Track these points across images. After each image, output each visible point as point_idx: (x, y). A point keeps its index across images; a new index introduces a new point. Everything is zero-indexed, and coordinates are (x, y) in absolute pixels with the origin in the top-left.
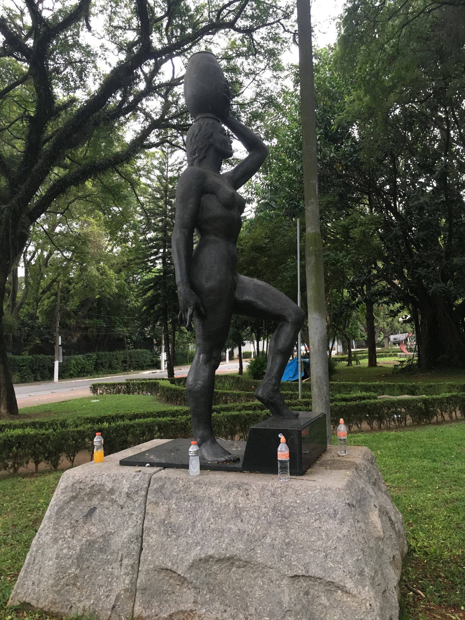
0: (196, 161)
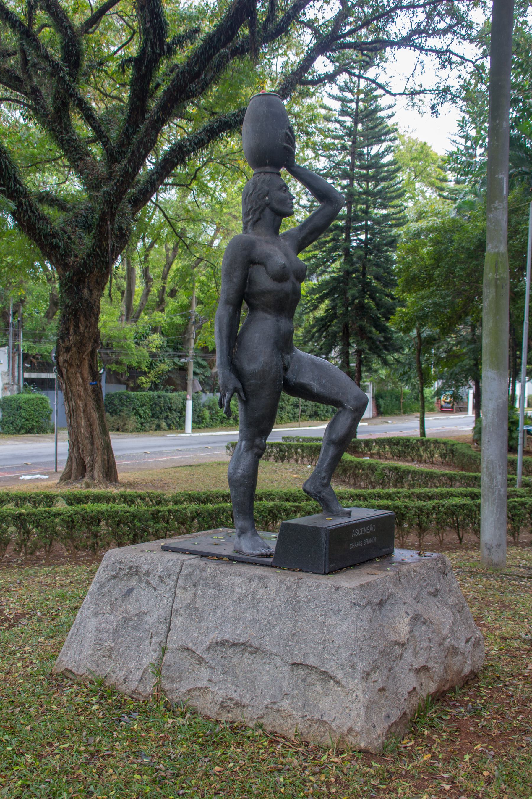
0: (250, 223)
